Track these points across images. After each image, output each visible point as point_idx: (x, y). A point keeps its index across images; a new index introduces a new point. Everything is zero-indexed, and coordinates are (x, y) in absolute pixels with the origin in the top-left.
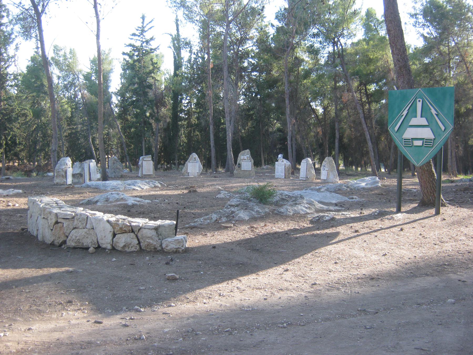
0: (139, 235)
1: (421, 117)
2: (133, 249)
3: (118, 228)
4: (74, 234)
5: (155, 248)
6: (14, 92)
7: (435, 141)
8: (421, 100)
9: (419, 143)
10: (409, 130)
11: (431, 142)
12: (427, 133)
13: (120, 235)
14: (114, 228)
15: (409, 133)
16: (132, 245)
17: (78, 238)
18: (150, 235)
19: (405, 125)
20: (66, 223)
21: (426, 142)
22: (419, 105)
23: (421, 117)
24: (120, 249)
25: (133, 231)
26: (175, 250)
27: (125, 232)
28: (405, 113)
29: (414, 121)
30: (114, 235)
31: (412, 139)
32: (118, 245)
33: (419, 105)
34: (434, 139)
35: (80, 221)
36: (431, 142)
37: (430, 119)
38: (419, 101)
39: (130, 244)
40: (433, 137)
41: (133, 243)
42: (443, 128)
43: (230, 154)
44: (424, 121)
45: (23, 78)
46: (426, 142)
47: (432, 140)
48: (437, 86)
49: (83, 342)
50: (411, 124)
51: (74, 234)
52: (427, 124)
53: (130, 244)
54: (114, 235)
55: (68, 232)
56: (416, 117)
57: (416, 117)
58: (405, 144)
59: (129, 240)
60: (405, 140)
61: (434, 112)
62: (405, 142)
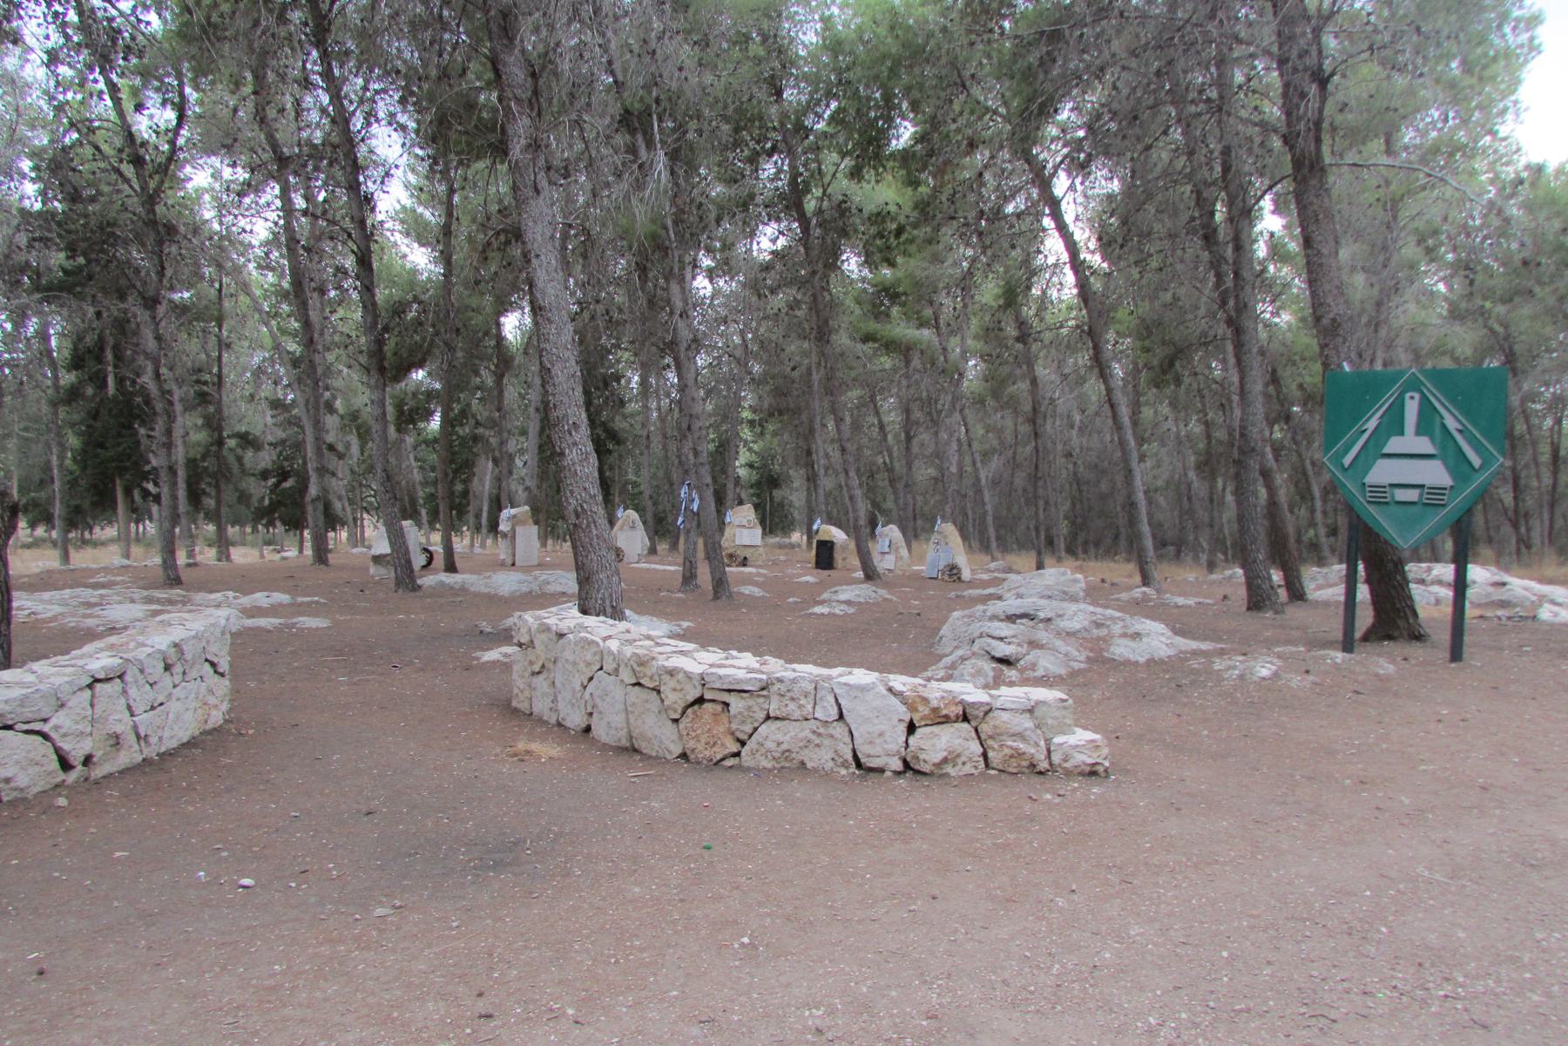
0: (985, 728)
2: (968, 769)
3: (924, 710)
4: (772, 737)
5: (1033, 766)
8: (1417, 396)
9: (1412, 495)
10: (1381, 463)
12: (1436, 474)
13: (928, 729)
14: (912, 708)
15: (1382, 473)
16: (964, 759)
17: (785, 747)
18: (1018, 729)
19: (1374, 450)
20: (737, 704)
24: (926, 768)
25: (965, 718)
26: (1088, 769)
27: (946, 720)
28: (1372, 424)
29: (1394, 445)
30: (911, 728)
31: (1392, 485)
32: (922, 756)
35: (793, 699)
39: (959, 756)
40: (1368, 480)
41: (967, 753)
42: (1476, 461)
44: (1424, 445)
48: (174, 249)
50: (1386, 450)
51: (772, 737)
53: (959, 756)
54: (911, 728)
55: (748, 728)
56: (1402, 434)
57: (1402, 434)
59: (957, 743)
61: (1451, 424)
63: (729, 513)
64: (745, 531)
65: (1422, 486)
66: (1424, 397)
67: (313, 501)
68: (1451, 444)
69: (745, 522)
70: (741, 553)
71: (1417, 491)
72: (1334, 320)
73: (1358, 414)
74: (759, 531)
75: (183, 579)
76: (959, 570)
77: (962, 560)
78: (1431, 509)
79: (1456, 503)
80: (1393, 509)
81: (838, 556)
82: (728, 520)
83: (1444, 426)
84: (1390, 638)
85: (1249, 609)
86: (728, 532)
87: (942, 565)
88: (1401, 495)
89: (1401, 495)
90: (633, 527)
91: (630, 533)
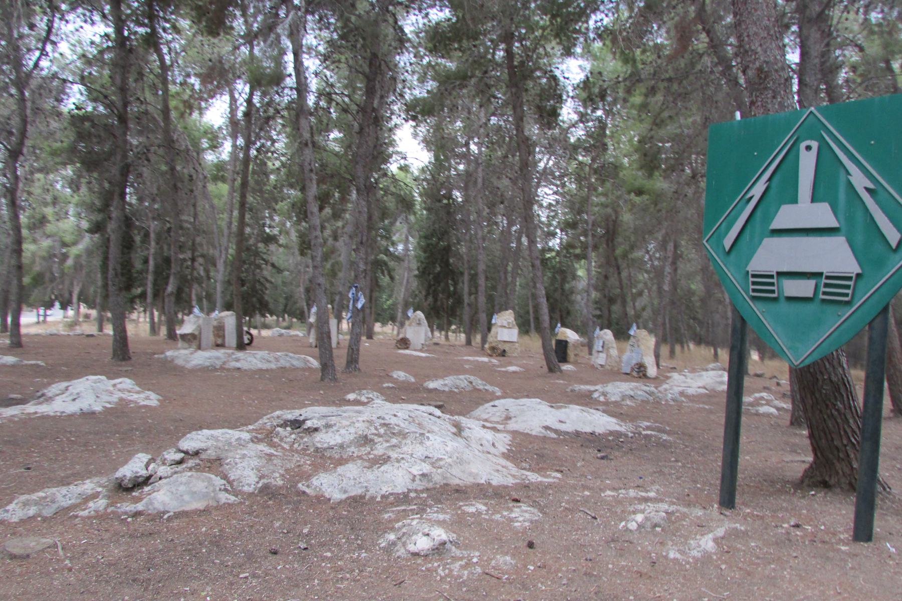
1: (813, 200)
6: (344, 101)
7: (861, 283)
8: (815, 145)
9: (805, 288)
10: (771, 243)
11: (848, 287)
12: (837, 257)
15: (770, 256)
19: (759, 226)
21: (826, 285)
22: (807, 163)
23: (813, 200)
28: (758, 190)
31: (779, 274)
33: (807, 163)
34: (858, 275)
36: (848, 287)
37: (850, 206)
38: (808, 148)
43: (483, 317)
45: (412, 101)
46: (826, 285)
47: (850, 278)
49: (357, 402)
50: (776, 224)
52: (834, 223)
56: (795, 200)
57: (795, 200)
58: (754, 291)
60: (754, 276)
61: (860, 181)
62: (754, 283)
63: (495, 316)
64: (505, 330)
65: (819, 275)
66: (824, 148)
67: (169, 295)
68: (859, 215)
69: (505, 324)
70: (501, 347)
71: (812, 283)
72: (760, 70)
73: (744, 179)
74: (516, 331)
75: (23, 343)
76: (645, 368)
77: (649, 361)
78: (830, 309)
79: (866, 297)
80: (783, 307)
81: (571, 353)
82: (493, 321)
83: (850, 185)
84: (825, 485)
85: (792, 423)
86: (493, 330)
87: (634, 362)
88: (792, 288)
89: (792, 288)
90: (419, 324)
91: (417, 328)
